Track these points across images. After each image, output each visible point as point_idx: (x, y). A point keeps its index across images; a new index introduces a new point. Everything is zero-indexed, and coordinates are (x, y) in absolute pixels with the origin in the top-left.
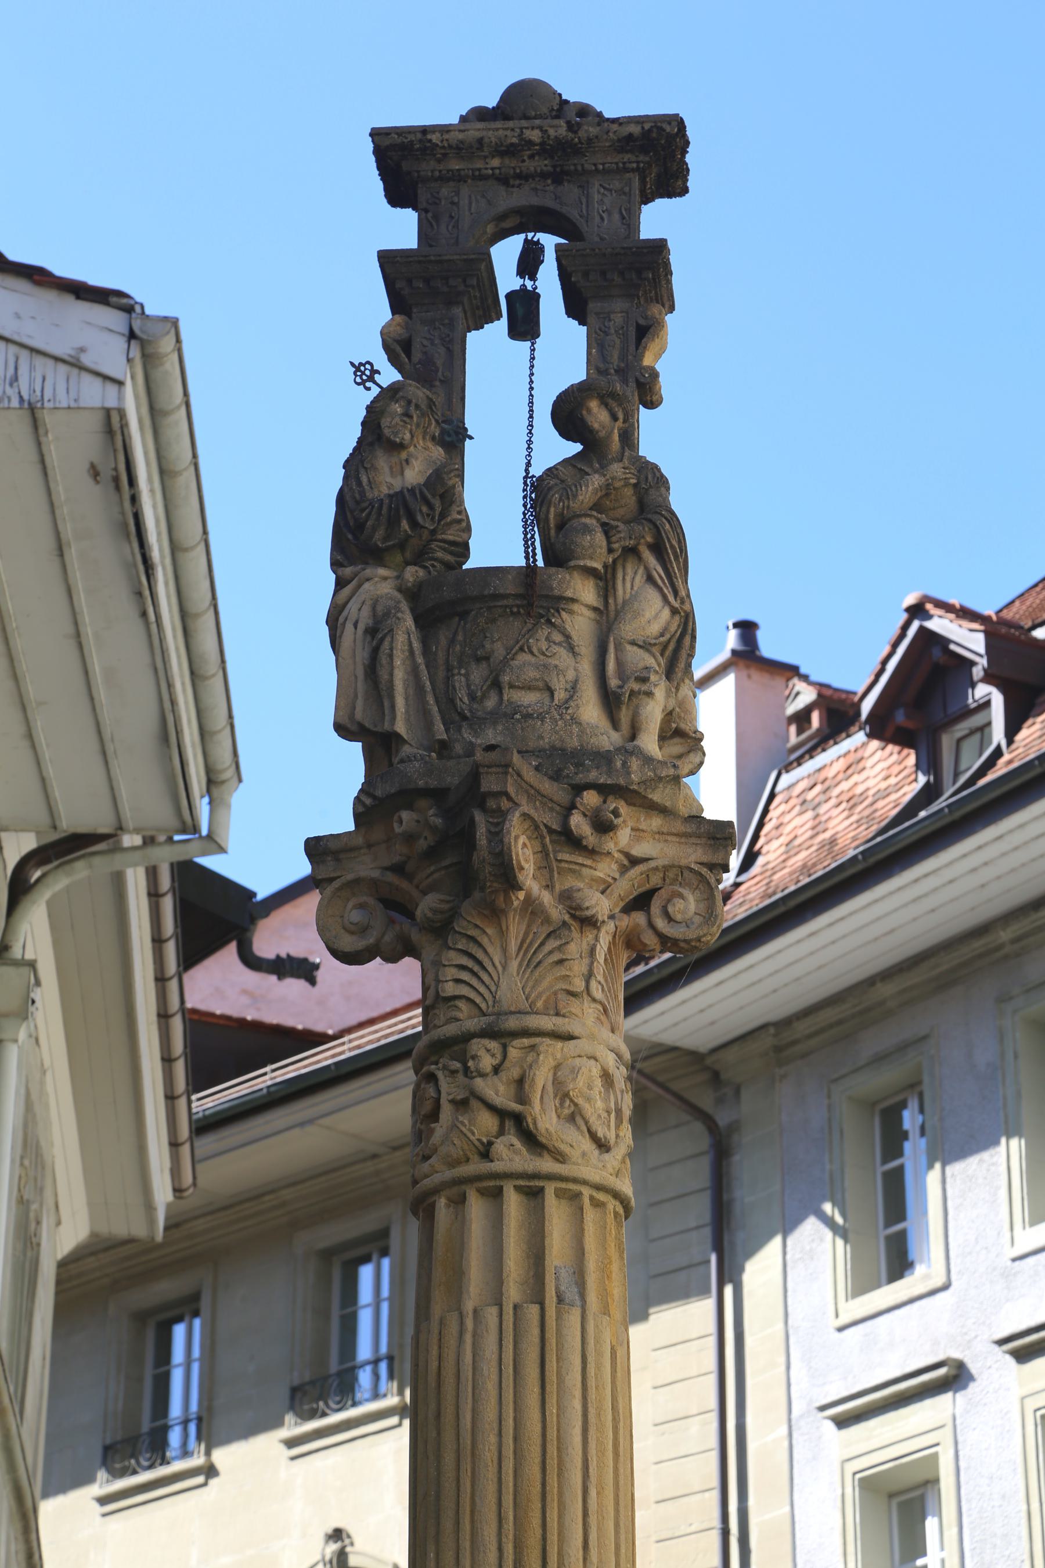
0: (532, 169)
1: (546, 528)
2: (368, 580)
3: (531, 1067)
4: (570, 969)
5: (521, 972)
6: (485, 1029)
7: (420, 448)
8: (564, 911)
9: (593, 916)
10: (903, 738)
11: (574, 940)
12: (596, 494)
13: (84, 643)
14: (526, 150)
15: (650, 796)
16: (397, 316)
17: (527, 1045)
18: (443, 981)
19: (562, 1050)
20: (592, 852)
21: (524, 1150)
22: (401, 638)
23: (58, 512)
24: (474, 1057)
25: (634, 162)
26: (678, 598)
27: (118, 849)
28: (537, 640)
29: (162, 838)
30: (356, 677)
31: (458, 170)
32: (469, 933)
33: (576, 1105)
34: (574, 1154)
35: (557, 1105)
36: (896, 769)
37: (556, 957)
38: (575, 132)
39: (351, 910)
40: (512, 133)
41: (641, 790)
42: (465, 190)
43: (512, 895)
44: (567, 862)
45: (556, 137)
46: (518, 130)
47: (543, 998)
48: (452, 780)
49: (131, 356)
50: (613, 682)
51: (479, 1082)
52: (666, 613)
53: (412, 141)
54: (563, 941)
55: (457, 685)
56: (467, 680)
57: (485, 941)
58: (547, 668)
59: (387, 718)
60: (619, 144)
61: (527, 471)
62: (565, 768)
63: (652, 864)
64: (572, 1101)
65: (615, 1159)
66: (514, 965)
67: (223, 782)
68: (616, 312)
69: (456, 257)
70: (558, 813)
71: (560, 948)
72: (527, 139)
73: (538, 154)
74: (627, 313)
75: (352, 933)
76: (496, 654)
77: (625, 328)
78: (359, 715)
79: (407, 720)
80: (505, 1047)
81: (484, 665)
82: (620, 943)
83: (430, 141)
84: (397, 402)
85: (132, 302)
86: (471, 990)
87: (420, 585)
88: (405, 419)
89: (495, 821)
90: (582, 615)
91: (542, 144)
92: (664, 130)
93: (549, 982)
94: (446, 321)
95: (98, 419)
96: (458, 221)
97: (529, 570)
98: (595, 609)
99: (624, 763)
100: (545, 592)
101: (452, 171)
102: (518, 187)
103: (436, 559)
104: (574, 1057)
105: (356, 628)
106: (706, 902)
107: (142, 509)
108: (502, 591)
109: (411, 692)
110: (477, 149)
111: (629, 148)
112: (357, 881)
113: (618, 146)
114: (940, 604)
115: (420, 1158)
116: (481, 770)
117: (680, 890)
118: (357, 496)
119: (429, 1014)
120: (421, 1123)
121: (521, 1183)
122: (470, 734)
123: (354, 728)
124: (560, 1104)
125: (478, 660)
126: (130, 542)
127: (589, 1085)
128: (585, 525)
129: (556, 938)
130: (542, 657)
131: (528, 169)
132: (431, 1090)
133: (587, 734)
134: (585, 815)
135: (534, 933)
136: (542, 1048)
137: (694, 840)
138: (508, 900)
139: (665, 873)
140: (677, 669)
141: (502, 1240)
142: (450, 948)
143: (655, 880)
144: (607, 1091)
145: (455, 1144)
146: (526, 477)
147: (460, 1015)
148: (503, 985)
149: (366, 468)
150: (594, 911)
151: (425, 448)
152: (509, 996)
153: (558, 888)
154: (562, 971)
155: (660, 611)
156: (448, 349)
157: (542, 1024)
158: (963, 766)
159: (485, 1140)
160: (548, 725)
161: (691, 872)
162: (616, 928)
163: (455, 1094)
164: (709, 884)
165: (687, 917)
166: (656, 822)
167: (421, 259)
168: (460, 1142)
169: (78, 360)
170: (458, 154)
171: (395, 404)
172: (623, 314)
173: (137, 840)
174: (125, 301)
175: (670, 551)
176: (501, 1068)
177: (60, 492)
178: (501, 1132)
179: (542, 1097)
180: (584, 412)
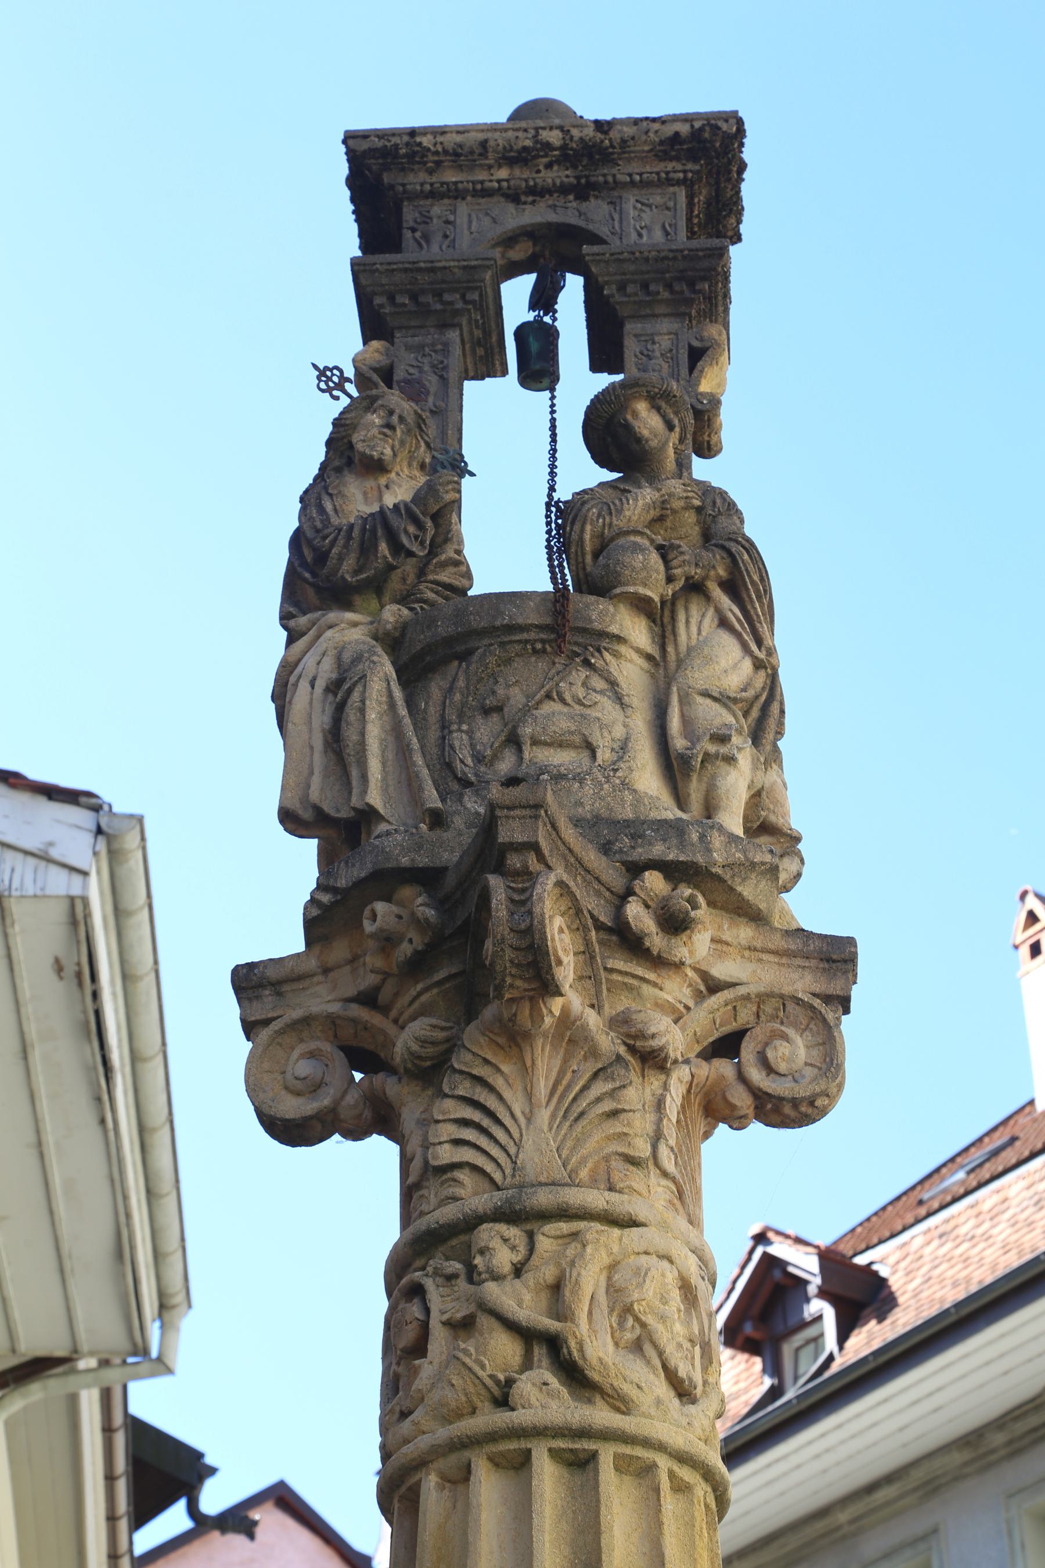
0: (550, 181)
1: (579, 553)
2: (330, 627)
3: (572, 1263)
4: (629, 1125)
5: (555, 1126)
6: (501, 1207)
7: (404, 476)
8: (619, 1041)
9: (662, 1049)
10: (751, 1347)
11: (634, 1084)
12: (648, 512)
13: (45, 1152)
14: (542, 157)
15: (739, 889)
16: (375, 344)
17: (566, 1232)
18: (434, 1144)
19: (621, 1240)
20: (659, 962)
21: (564, 1392)
22: (376, 688)
23: (23, 1010)
24: (482, 1252)
25: (679, 171)
26: (763, 649)
27: (74, 1371)
28: (570, 683)
29: (117, 1361)
30: (312, 748)
31: (456, 183)
32: (475, 1072)
33: (643, 1325)
34: (644, 1400)
35: (615, 1325)
36: (744, 1375)
37: (607, 1106)
38: (606, 133)
39: (297, 1061)
40: (525, 134)
41: (727, 877)
42: (463, 208)
43: (542, 1005)
44: (620, 972)
45: (581, 138)
46: (533, 132)
47: (590, 1165)
48: (449, 857)
49: (97, 848)
50: (679, 743)
51: (492, 1290)
52: (747, 665)
53: (396, 145)
54: (618, 1084)
55: (457, 743)
56: (471, 738)
57: (499, 1083)
58: (585, 718)
59: (355, 791)
60: (662, 148)
61: (550, 496)
62: (617, 840)
63: (742, 990)
64: (637, 1319)
65: (706, 1415)
66: (544, 1116)
67: (173, 1307)
68: (661, 334)
69: (452, 264)
70: (606, 901)
71: (612, 1094)
72: (545, 141)
73: (558, 162)
74: (676, 334)
75: (298, 1094)
76: (512, 702)
77: (674, 351)
78: (315, 795)
79: (385, 790)
80: (531, 1236)
81: (495, 717)
82: (696, 1102)
83: (420, 144)
84: (375, 412)
85: (100, 802)
86: (478, 1154)
87: (404, 627)
88: (385, 430)
89: (520, 886)
90: (631, 661)
91: (564, 148)
92: (719, 128)
93: (598, 1142)
94: (439, 347)
95: (62, 908)
96: (454, 239)
97: (558, 594)
98: (649, 658)
99: (702, 837)
100: (580, 624)
101: (447, 184)
102: (530, 204)
103: (425, 601)
104: (638, 1254)
105: (313, 687)
106: (821, 1048)
107: (102, 1007)
108: (520, 621)
109: (390, 756)
110: (480, 155)
111: (673, 153)
112: (306, 1021)
113: (660, 151)
114: (778, 1233)
115: (397, 1415)
116: (498, 813)
117: (783, 1028)
118: (319, 525)
119: (411, 1198)
120: (398, 1364)
121: (561, 1444)
122: (475, 802)
123: (307, 815)
124: (619, 1324)
125: (487, 712)
126: (90, 1041)
127: (662, 1297)
128: (635, 543)
129: (606, 1080)
130: (577, 707)
131: (544, 181)
132: (415, 1308)
133: (644, 805)
134: (647, 907)
135: (573, 1072)
136: (589, 1236)
137: (798, 961)
138: (537, 1017)
139: (759, 1007)
140: (764, 741)
141: (531, 1537)
142: (446, 1096)
143: (746, 1016)
144: (688, 1311)
145: (453, 1385)
146: (548, 505)
147: (460, 1192)
148: (528, 1143)
149: (331, 495)
150: (664, 1040)
151: (411, 477)
152: (536, 1160)
153: (608, 1011)
154: (616, 1127)
155: (740, 661)
156: (441, 377)
157: (589, 1200)
158: (801, 1371)
159: (501, 1377)
160: (589, 789)
161: (798, 1004)
162: (693, 1076)
163: (453, 1311)
164: (824, 1020)
165: (795, 1067)
166: (745, 933)
167: (407, 266)
168: (461, 1381)
169: (46, 853)
170: (453, 161)
171: (373, 414)
172: (671, 337)
173: (93, 1363)
174: (93, 801)
175: (750, 587)
176: (526, 1268)
177: (26, 990)
178: (527, 1364)
179: (590, 1313)
180: (629, 417)
